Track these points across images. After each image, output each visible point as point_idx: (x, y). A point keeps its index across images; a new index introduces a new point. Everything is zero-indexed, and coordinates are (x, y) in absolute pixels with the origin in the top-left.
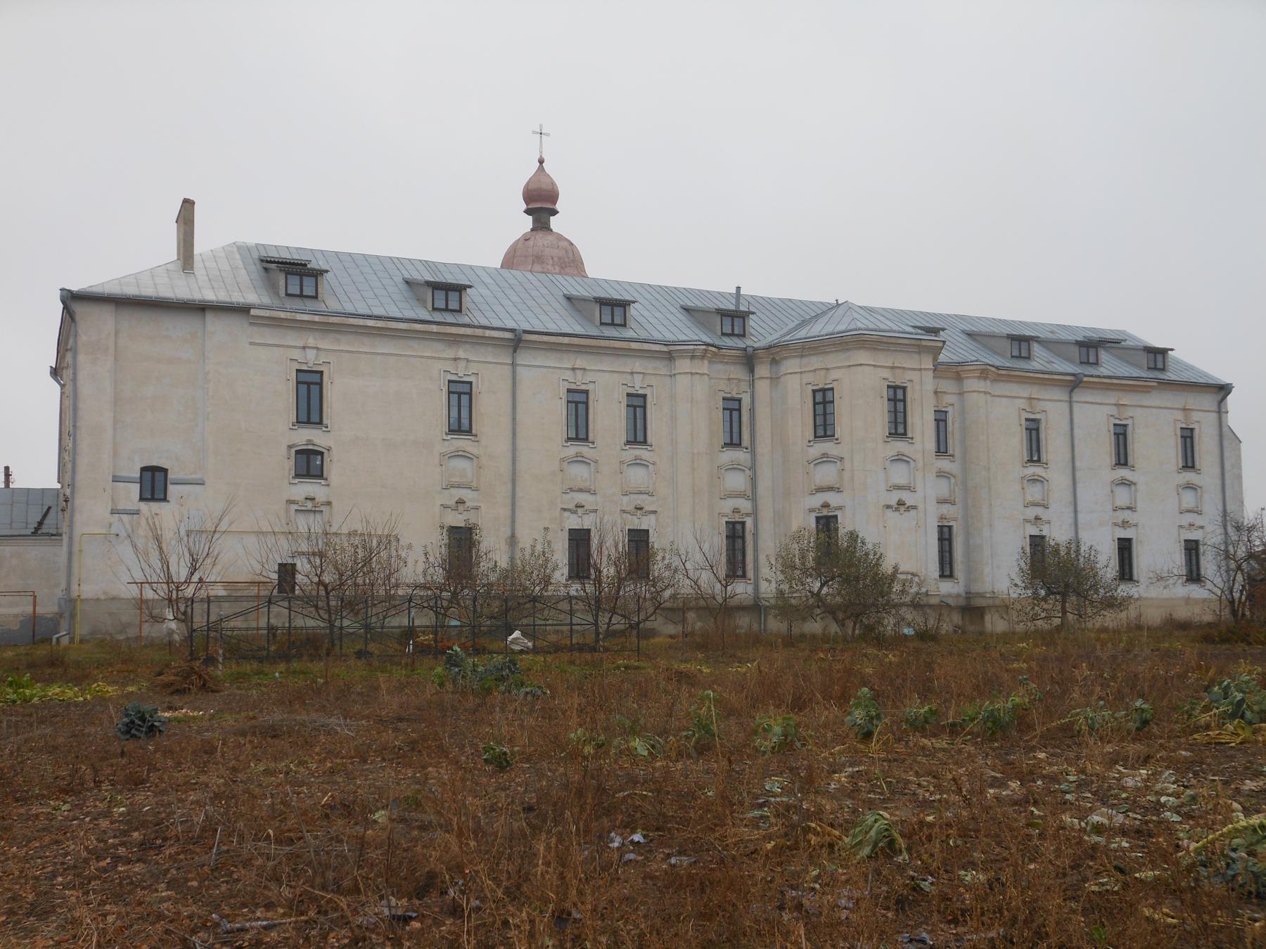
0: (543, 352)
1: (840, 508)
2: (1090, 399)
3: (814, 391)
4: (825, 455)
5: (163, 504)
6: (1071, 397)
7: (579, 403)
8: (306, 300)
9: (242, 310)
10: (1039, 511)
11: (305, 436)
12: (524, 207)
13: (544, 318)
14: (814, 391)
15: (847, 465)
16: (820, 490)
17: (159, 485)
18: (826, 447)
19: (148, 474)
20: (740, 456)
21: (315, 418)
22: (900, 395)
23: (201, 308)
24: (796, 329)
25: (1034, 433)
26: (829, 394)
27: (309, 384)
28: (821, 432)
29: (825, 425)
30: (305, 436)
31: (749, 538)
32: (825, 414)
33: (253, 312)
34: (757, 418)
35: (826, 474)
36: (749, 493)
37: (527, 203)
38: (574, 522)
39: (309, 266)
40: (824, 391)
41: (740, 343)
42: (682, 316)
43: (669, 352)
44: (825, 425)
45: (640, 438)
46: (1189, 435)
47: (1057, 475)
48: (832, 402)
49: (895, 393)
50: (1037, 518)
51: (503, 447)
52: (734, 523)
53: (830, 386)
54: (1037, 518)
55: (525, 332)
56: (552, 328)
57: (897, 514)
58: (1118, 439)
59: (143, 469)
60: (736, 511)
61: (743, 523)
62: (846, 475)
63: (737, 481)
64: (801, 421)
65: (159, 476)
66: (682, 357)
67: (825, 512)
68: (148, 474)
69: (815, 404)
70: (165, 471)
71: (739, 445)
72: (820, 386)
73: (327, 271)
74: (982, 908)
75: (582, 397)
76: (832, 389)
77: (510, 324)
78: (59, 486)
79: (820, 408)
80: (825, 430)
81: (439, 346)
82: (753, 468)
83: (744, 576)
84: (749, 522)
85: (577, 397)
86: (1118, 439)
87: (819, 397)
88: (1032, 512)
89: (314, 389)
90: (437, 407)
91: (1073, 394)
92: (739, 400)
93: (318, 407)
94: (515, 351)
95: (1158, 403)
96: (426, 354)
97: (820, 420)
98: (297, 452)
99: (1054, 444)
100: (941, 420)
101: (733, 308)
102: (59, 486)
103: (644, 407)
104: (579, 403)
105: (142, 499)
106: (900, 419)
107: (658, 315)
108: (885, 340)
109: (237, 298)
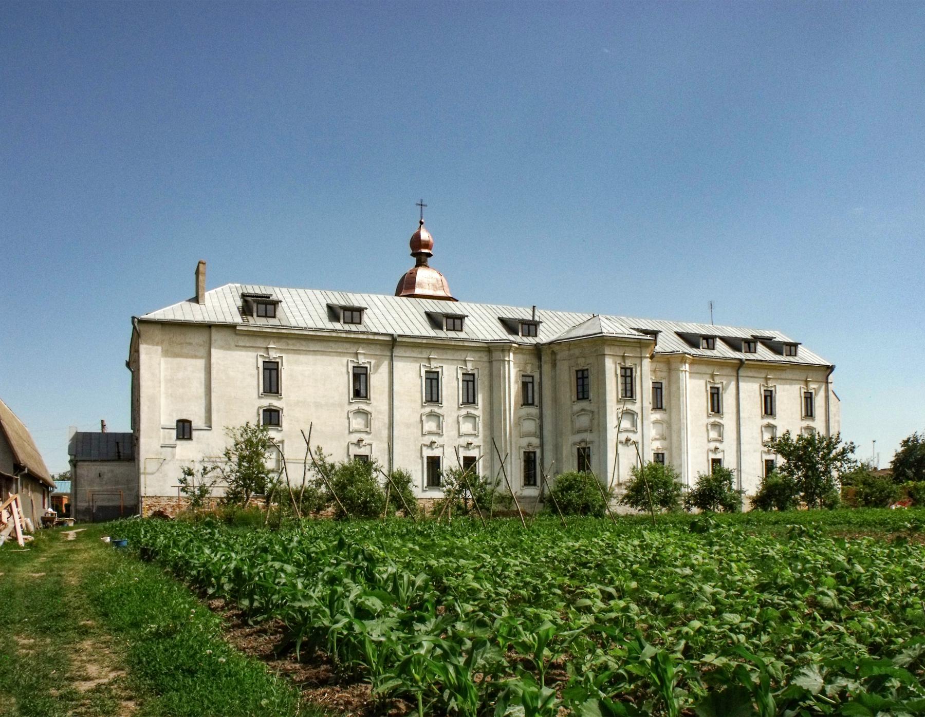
0: (410, 348)
1: (592, 442)
2: (750, 374)
3: (577, 371)
4: (583, 410)
5: (190, 442)
6: (738, 374)
7: (433, 380)
8: (269, 319)
9: (232, 327)
10: (718, 445)
11: (270, 402)
12: (411, 252)
13: (412, 327)
14: (577, 371)
15: (596, 416)
16: (579, 432)
17: (187, 430)
18: (584, 404)
19: (181, 424)
20: (534, 411)
21: (274, 389)
22: (628, 373)
23: (208, 327)
24: (570, 331)
25: (809, 400)
26: (586, 373)
27: (270, 370)
28: (581, 396)
29: (583, 392)
30: (270, 402)
31: (538, 461)
32: (583, 385)
33: (238, 328)
34: (543, 389)
35: (584, 421)
36: (538, 433)
37: (412, 249)
38: (427, 453)
39: (271, 298)
40: (583, 371)
41: (531, 340)
42: (499, 325)
43: (488, 347)
44: (583, 392)
45: (434, 399)
46: (716, 391)
47: (728, 419)
48: (587, 377)
49: (626, 373)
50: (717, 449)
51: (385, 407)
52: (529, 453)
53: (586, 368)
54: (717, 449)
55: (399, 336)
56: (417, 333)
57: (626, 447)
58: (468, 385)
59: (178, 421)
60: (583, 441)
61: (535, 453)
62: (595, 422)
63: (530, 426)
64: (568, 391)
65: (187, 424)
66: (496, 350)
67: (583, 445)
68: (181, 424)
69: (577, 378)
70: (190, 422)
71: (533, 404)
72: (580, 368)
73: (281, 301)
74: (247, 434)
75: (435, 376)
76: (587, 370)
77: (391, 331)
78: (132, 431)
79: (580, 381)
80: (583, 395)
81: (347, 345)
82: (541, 417)
83: (535, 484)
84: (538, 451)
85: (432, 376)
86: (468, 385)
87: (580, 375)
88: (713, 445)
89: (274, 373)
90: (343, 383)
91: (394, 350)
92: (533, 377)
93: (275, 384)
94: (393, 348)
95: (790, 377)
96: (339, 351)
97: (580, 389)
98: (264, 411)
99: (728, 400)
100: (657, 389)
101: (531, 319)
102: (132, 431)
103: (474, 381)
104: (433, 380)
105: (178, 438)
106: (629, 388)
107: (484, 324)
108: (624, 339)
109: (229, 320)
